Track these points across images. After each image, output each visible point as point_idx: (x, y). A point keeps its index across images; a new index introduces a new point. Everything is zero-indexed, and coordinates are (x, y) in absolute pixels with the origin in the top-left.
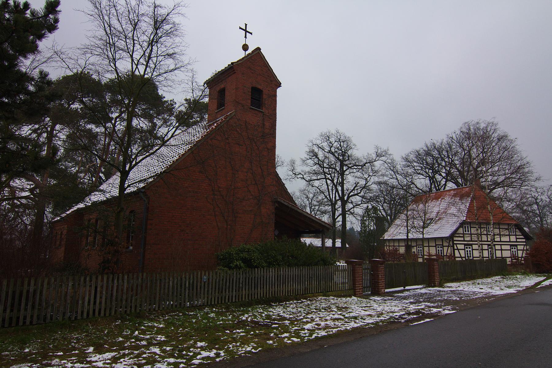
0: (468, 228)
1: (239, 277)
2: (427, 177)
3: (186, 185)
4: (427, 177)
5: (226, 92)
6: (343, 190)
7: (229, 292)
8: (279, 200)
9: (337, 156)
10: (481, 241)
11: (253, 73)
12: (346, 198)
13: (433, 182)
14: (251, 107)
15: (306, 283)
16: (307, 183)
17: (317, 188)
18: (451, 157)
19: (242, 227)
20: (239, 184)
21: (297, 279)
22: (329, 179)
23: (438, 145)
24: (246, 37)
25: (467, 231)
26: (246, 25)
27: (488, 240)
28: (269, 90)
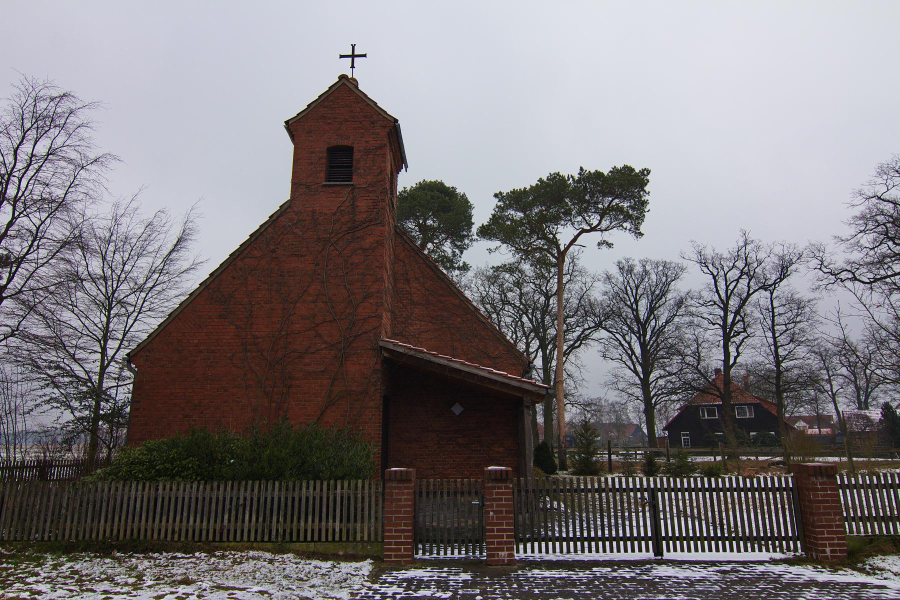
3: (195, 341)
11: (329, 124)
15: (226, 517)
19: (302, 403)
20: (298, 326)
21: (338, 510)
28: (366, 142)
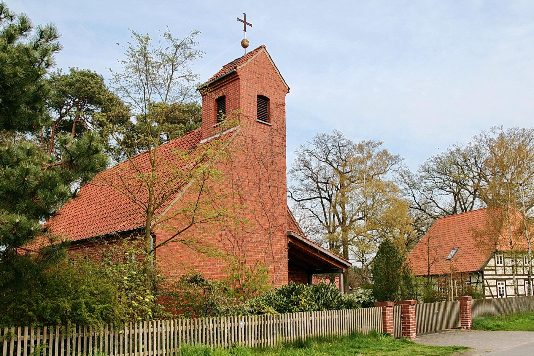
0: (501, 259)
1: (213, 327)
2: (451, 192)
4: (451, 192)
5: (227, 102)
6: (343, 213)
7: (264, 339)
8: (293, 234)
9: (336, 166)
10: (517, 275)
12: (348, 222)
13: (459, 199)
14: (258, 120)
16: (297, 203)
17: (310, 210)
18: (480, 166)
22: (325, 198)
23: (463, 148)
24: (245, 30)
25: (499, 262)
26: (245, 15)
27: (525, 273)
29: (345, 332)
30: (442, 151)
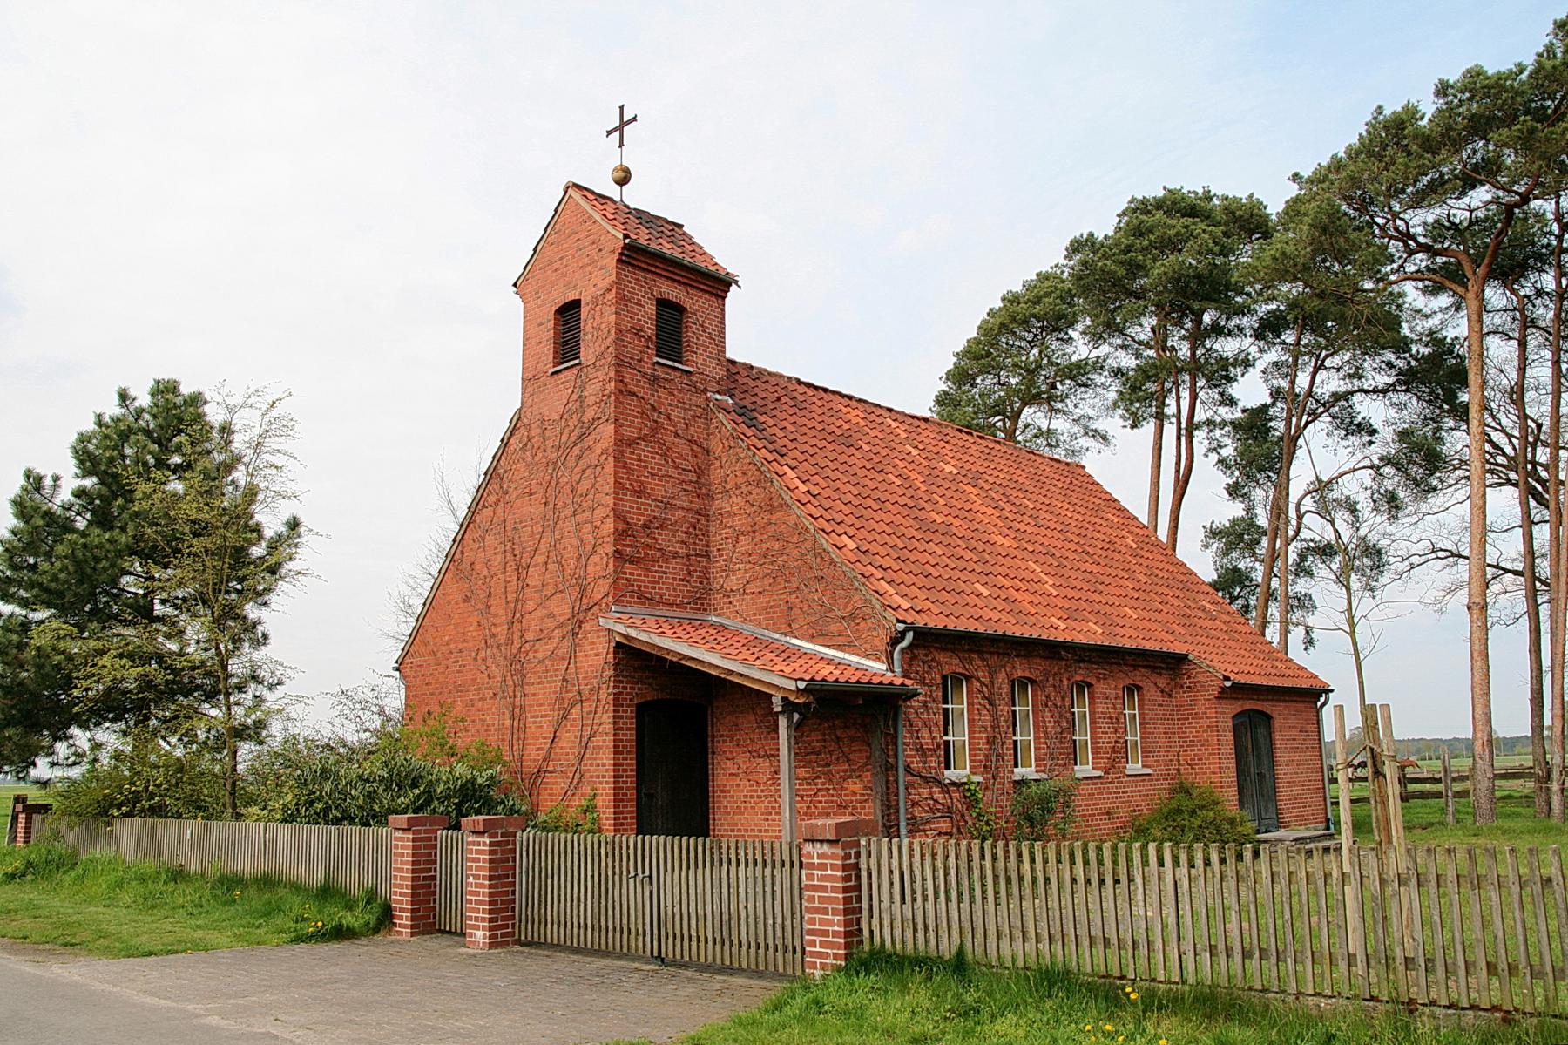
29: (316, 879)
30: (1067, 243)
